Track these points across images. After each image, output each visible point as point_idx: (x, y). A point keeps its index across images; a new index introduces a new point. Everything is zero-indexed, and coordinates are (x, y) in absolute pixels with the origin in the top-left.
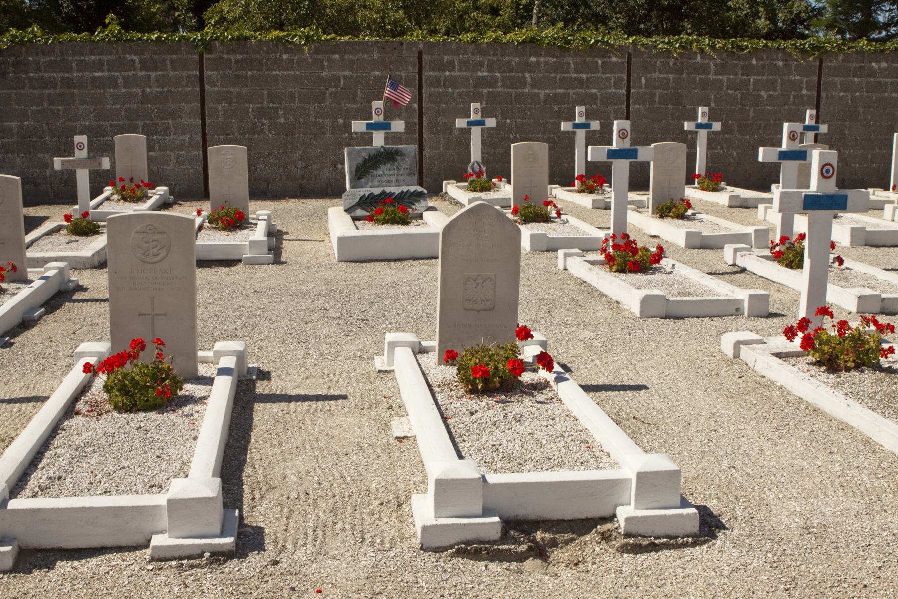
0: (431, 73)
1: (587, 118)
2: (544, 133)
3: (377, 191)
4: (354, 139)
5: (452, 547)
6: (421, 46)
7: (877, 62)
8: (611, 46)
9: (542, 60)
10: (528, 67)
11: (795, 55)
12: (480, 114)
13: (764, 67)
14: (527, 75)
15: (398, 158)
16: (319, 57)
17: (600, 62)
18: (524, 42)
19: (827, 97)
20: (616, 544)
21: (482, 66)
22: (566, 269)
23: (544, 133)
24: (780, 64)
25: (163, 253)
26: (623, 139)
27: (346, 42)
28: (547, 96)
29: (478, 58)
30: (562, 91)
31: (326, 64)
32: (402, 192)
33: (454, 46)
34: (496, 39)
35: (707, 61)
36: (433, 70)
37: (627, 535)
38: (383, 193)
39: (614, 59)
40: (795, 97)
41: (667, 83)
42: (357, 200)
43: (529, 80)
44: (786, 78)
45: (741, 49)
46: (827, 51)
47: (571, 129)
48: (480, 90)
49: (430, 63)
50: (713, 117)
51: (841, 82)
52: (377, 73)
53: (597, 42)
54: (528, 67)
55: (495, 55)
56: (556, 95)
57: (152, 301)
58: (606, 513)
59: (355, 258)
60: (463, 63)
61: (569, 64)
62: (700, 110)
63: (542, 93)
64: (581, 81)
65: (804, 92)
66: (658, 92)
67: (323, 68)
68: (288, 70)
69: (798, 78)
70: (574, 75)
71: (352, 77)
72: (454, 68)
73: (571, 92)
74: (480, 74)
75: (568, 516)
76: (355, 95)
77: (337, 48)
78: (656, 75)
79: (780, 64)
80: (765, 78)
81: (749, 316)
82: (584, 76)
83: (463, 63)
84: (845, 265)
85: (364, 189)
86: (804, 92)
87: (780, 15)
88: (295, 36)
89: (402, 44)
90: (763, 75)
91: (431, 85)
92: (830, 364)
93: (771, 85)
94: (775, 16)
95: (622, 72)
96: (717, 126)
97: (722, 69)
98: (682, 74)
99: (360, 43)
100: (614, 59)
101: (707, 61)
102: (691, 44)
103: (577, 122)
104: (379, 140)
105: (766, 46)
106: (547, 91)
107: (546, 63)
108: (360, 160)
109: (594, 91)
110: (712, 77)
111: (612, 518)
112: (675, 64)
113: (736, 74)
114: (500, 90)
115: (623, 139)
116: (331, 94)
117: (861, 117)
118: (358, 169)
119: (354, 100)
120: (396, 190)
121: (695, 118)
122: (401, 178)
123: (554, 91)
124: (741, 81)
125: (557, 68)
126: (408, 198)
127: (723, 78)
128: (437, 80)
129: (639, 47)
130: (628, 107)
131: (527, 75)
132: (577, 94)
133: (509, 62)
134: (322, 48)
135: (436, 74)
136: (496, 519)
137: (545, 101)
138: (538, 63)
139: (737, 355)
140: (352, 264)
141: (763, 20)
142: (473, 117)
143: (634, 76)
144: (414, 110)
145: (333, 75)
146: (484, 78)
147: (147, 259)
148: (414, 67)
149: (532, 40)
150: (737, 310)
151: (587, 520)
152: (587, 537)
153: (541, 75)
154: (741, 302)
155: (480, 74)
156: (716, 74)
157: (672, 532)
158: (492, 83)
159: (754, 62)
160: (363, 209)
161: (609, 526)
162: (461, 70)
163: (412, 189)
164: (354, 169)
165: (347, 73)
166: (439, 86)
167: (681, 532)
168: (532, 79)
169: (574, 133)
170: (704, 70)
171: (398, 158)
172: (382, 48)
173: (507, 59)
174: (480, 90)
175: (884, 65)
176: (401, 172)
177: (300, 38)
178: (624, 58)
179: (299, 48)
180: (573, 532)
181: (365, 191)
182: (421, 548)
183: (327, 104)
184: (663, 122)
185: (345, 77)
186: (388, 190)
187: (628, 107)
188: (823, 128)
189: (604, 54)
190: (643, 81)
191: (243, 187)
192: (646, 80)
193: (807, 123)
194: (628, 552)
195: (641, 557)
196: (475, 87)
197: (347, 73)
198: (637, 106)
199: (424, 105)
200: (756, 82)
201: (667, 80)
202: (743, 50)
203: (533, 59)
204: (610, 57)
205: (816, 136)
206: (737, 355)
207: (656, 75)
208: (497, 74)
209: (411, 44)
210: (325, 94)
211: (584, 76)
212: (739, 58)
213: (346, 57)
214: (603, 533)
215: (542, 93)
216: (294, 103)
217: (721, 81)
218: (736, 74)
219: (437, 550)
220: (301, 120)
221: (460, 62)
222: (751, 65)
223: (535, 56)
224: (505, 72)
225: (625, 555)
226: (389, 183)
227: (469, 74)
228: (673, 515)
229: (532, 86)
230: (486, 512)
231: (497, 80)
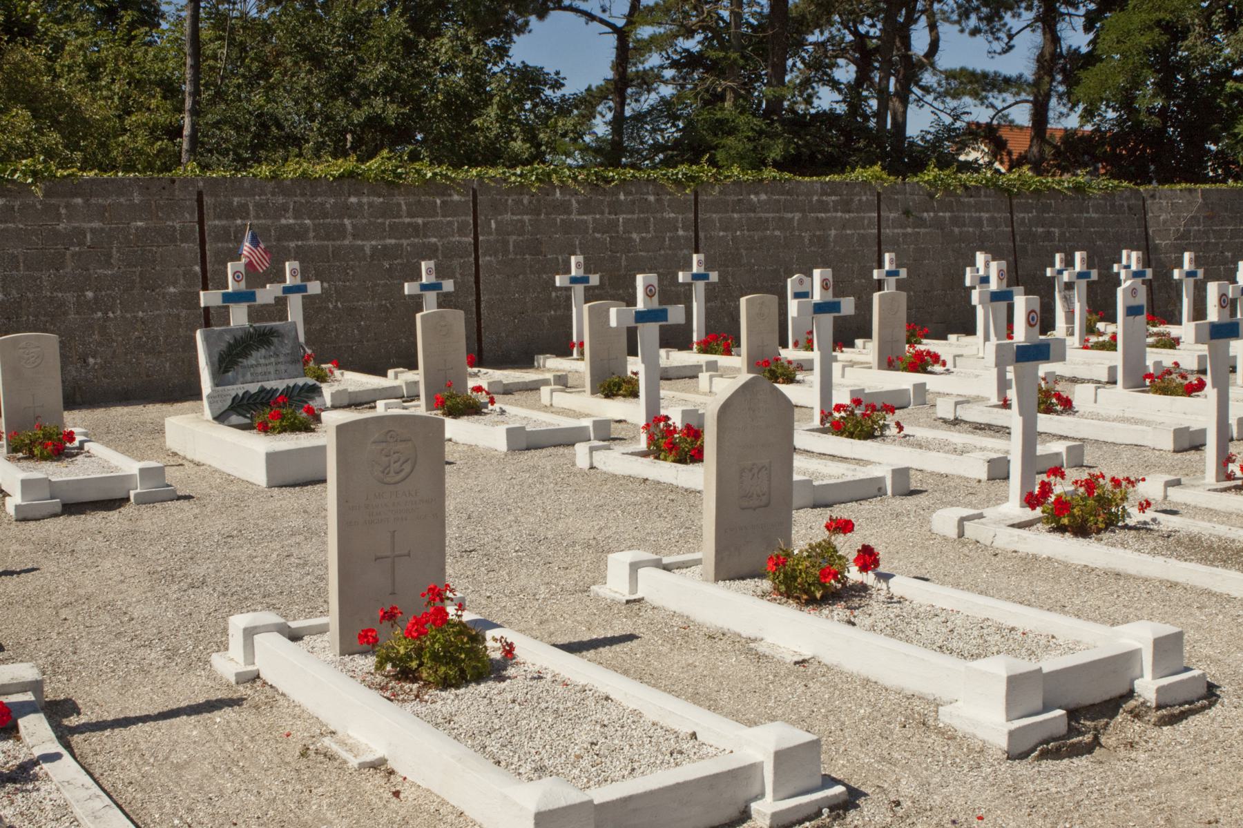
0: (217, 222)
1: (585, 272)
2: (373, 299)
3: (253, 388)
4: (111, 320)
5: (1034, 750)
6: (201, 184)
7: (757, 194)
8: (453, 180)
9: (365, 200)
10: (346, 211)
11: (671, 187)
12: (299, 277)
13: (633, 202)
14: (346, 221)
15: (275, 340)
16: (53, 201)
17: (438, 202)
18: (341, 176)
19: (706, 238)
20: (1153, 716)
21: (286, 211)
22: (592, 467)
23: (373, 299)
24: (652, 198)
25: (407, 468)
26: (651, 297)
27: (92, 180)
28: (374, 248)
29: (281, 200)
30: (393, 241)
31: (63, 211)
32: (288, 387)
33: (246, 185)
34: (304, 173)
35: (567, 198)
36: (219, 218)
37: (1159, 707)
38: (262, 390)
39: (456, 197)
40: (671, 239)
41: (523, 226)
42: (229, 402)
43: (349, 227)
44: (659, 215)
45: (608, 181)
46: (703, 182)
47: (419, 292)
48: (286, 244)
49: (215, 207)
50: (589, 268)
51: (720, 219)
52: (139, 224)
53: (435, 174)
54: (346, 211)
55: (303, 195)
56: (385, 247)
57: (393, 536)
58: (1122, 689)
59: (290, 480)
60: (259, 206)
61: (399, 205)
62: (424, 265)
63: (368, 245)
64: (416, 227)
65: (681, 233)
66: (512, 238)
67: (58, 217)
68: (6, 222)
69: (672, 215)
70: (407, 220)
71: (102, 229)
72: (248, 214)
73: (405, 242)
74: (283, 221)
75: (1098, 701)
76: (109, 256)
77: (78, 188)
78: (508, 217)
79: (652, 198)
80: (636, 216)
81: (894, 495)
82: (420, 221)
83: (259, 206)
84: (905, 431)
85: (235, 387)
86: (681, 233)
87: (541, 135)
88: (15, 171)
89: (173, 181)
90: (633, 213)
91: (217, 239)
92: (1081, 530)
93: (643, 225)
94: (535, 137)
95: (467, 215)
96: (714, 277)
97: (586, 207)
98: (539, 214)
99: (113, 180)
100: (456, 197)
101: (567, 198)
102: (549, 175)
103: (424, 281)
104: (239, 317)
105: (633, 176)
106: (373, 243)
107: (371, 205)
108: (223, 346)
109: (434, 240)
110: (574, 217)
111: (1130, 694)
112: (530, 202)
113: (602, 213)
114: (311, 242)
115: (651, 297)
116: (73, 255)
117: (745, 261)
118: (222, 359)
119: (108, 265)
120: (279, 385)
121: (568, 271)
122: (282, 367)
123: (382, 242)
124: (609, 220)
125: (385, 211)
126: (299, 395)
127: (588, 218)
128: (226, 230)
129: (487, 181)
130: (477, 259)
131: (346, 221)
132: (413, 245)
133: (322, 204)
134: (55, 188)
135: (224, 222)
136: (1059, 712)
137: (372, 256)
138: (360, 204)
139: (961, 534)
140: (286, 491)
141: (519, 143)
142: (289, 281)
143: (481, 218)
144: (196, 274)
145: (75, 228)
146: (289, 227)
147: (388, 479)
148: (192, 215)
149: (351, 175)
150: (880, 489)
151: (1111, 700)
152: (1119, 718)
153: (364, 221)
154: (881, 480)
155: (283, 221)
156: (579, 213)
157: (1188, 697)
158: (301, 234)
159: (622, 197)
160: (239, 414)
161: (1132, 703)
162: (257, 217)
163: (301, 381)
164: (216, 359)
165: (96, 225)
166: (228, 240)
167: (1195, 696)
168: (354, 226)
169: (420, 297)
170: (565, 208)
171: (275, 340)
172: (145, 188)
173: (319, 199)
174: (286, 244)
175: (763, 197)
176: (282, 359)
177: (24, 173)
178: (468, 195)
179: (23, 189)
180: (1103, 716)
181: (238, 389)
182: (1008, 758)
183: (68, 270)
184: (521, 277)
185: (92, 230)
186: (269, 385)
187: (477, 259)
188: (595, 280)
189: (444, 191)
190: (493, 225)
191: (55, 394)
192: (496, 222)
193: (573, 273)
194: (1166, 725)
195: (1181, 726)
196: (278, 239)
197: (96, 225)
198: (488, 258)
199: (209, 267)
200: (626, 222)
201: (522, 221)
202: (609, 182)
203: (353, 200)
204: (450, 195)
205: (586, 289)
206: (961, 534)
207: (508, 217)
208: (307, 221)
209: (187, 182)
210: (64, 254)
211: (420, 221)
212: (605, 192)
213: (93, 201)
214: (1131, 712)
215: (368, 245)
216: (17, 268)
217: (586, 222)
218: (602, 213)
219: (1023, 756)
220: (30, 295)
221: (257, 205)
222: (618, 200)
223: (355, 195)
224: (316, 218)
225: (1165, 728)
226: (266, 376)
227: (269, 222)
228: (1170, 685)
229: (355, 236)
230: (1046, 708)
231: (307, 230)
